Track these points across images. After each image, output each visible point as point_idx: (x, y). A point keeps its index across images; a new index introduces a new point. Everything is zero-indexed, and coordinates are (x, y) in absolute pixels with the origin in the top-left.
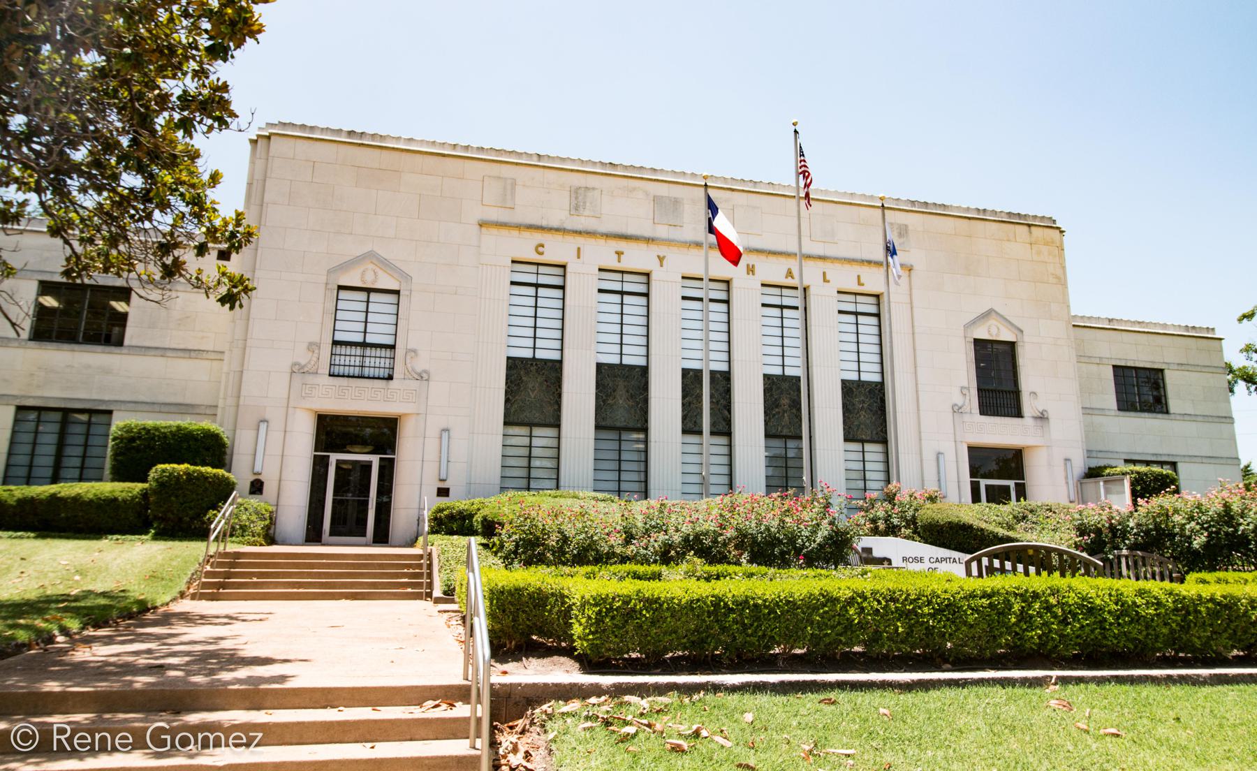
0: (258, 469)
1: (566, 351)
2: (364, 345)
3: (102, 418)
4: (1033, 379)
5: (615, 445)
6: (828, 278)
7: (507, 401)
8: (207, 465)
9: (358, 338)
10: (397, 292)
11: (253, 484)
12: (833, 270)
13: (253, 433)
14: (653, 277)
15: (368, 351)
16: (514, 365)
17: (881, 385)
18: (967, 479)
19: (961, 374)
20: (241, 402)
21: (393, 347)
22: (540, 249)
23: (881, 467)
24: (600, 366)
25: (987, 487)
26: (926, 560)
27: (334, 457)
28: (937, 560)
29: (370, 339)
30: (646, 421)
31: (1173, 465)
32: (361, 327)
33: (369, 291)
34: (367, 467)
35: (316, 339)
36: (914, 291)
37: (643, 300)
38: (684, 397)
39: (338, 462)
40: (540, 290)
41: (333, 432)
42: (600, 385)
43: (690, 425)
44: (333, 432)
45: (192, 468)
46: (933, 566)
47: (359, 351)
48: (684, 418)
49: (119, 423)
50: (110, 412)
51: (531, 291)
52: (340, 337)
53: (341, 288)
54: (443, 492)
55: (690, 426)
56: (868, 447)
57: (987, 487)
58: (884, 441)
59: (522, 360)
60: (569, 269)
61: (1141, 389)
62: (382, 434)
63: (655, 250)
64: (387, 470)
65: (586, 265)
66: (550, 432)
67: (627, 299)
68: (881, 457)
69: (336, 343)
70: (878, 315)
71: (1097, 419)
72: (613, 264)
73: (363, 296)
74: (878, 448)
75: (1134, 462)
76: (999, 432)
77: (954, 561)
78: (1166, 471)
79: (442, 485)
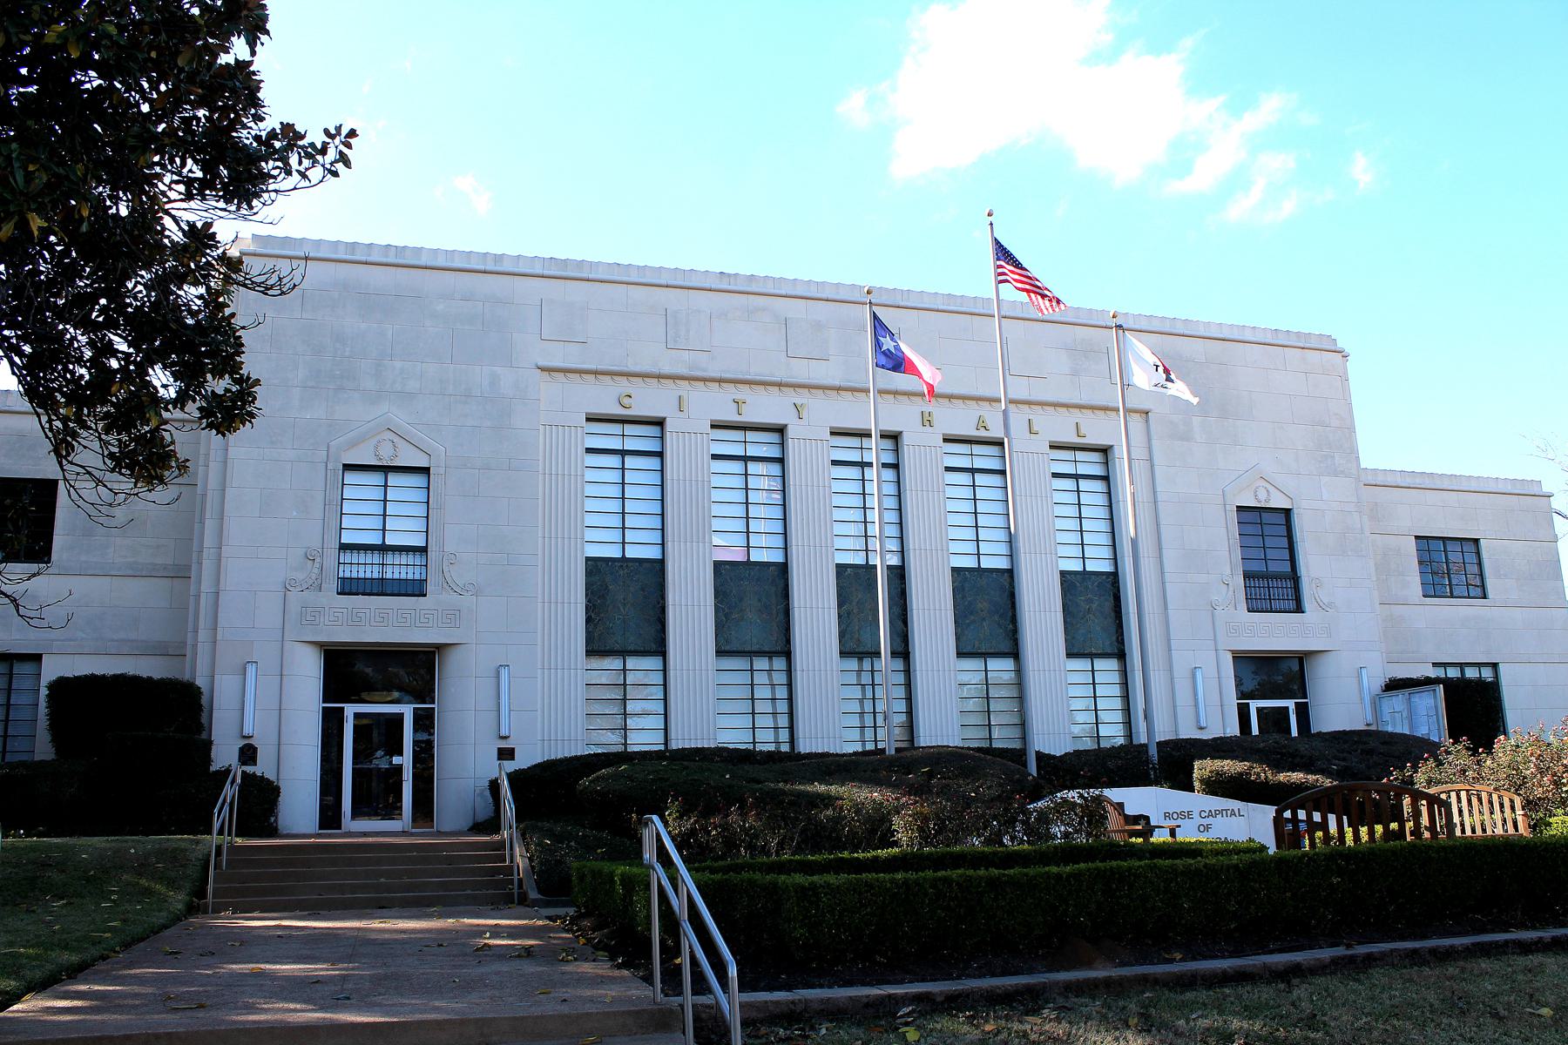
0: (247, 730)
1: (669, 545)
2: (383, 548)
3: (27, 668)
4: (1316, 564)
5: (745, 678)
6: (1035, 429)
7: (588, 620)
8: (1070, 875)
9: (373, 539)
10: (425, 471)
11: (242, 750)
12: (1041, 418)
13: (239, 678)
14: (791, 432)
15: (389, 558)
16: (596, 568)
17: (1010, 573)
18: (1232, 701)
19: (1221, 558)
20: (219, 637)
21: (423, 550)
22: (626, 401)
23: (1117, 690)
24: (718, 565)
25: (1259, 710)
26: (1195, 815)
27: (350, 710)
28: (1210, 814)
29: (391, 540)
30: (788, 641)
31: (1495, 666)
32: (378, 524)
33: (386, 470)
34: (399, 718)
35: (315, 543)
36: (1154, 442)
37: (654, 463)
38: (840, 606)
39: (357, 716)
40: (627, 459)
41: (346, 671)
42: (720, 593)
43: (851, 645)
44: (346, 671)
45: (971, 872)
46: (1206, 822)
47: (377, 558)
48: (842, 635)
49: (52, 669)
50: (37, 658)
51: (614, 461)
52: (347, 538)
53: (348, 467)
54: (506, 754)
55: (856, 647)
56: (1100, 664)
57: (1259, 710)
58: (1121, 655)
59: (733, 564)
60: (669, 426)
61: (1450, 565)
62: (415, 669)
63: (792, 397)
64: (424, 721)
65: (692, 418)
66: (653, 663)
67: (630, 462)
68: (1116, 678)
69: (344, 547)
70: (1105, 478)
71: (1398, 610)
72: (732, 417)
73: (377, 479)
74: (1113, 664)
75: (1445, 665)
76: (1275, 633)
77: (1233, 813)
78: (1487, 674)
79: (504, 744)
